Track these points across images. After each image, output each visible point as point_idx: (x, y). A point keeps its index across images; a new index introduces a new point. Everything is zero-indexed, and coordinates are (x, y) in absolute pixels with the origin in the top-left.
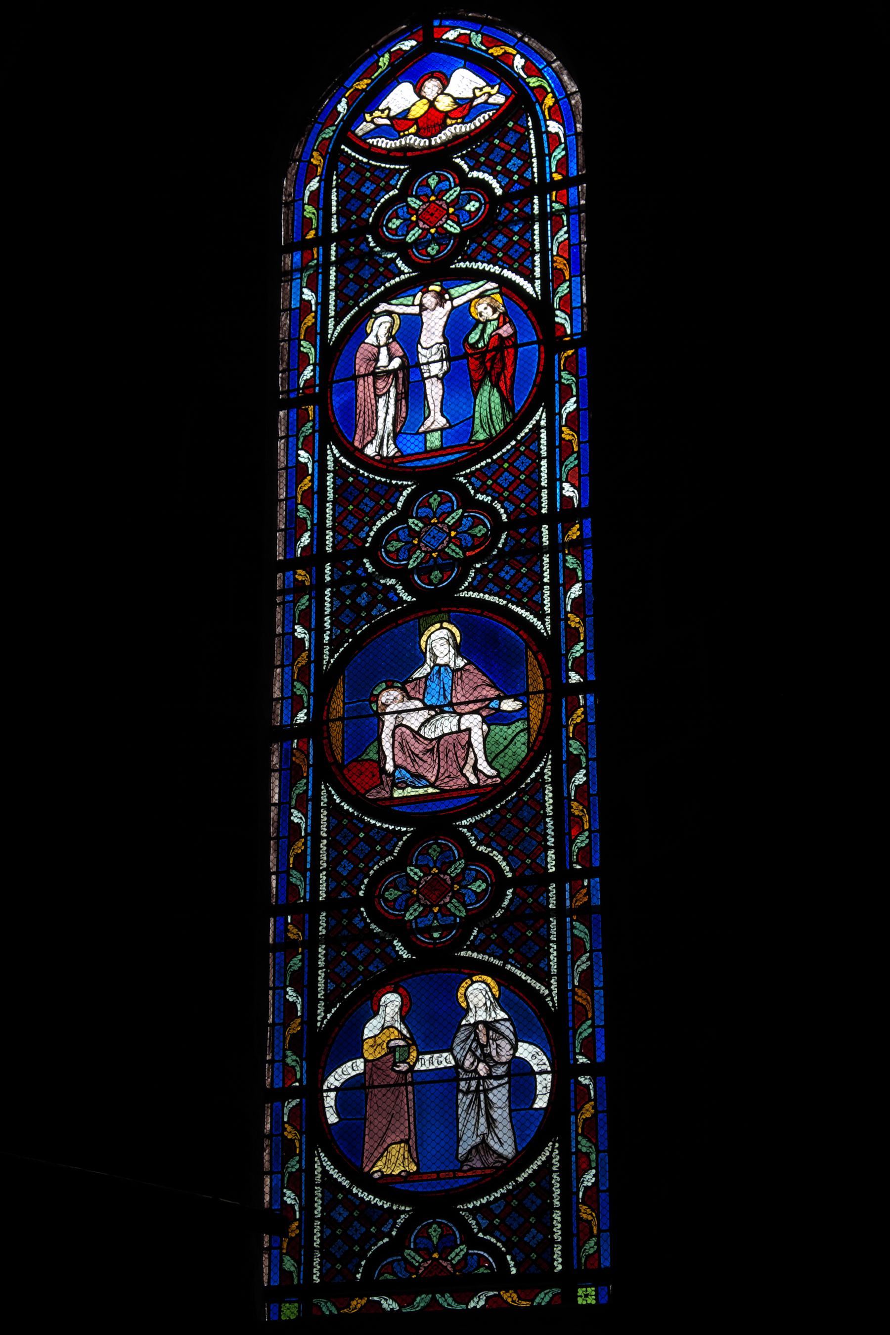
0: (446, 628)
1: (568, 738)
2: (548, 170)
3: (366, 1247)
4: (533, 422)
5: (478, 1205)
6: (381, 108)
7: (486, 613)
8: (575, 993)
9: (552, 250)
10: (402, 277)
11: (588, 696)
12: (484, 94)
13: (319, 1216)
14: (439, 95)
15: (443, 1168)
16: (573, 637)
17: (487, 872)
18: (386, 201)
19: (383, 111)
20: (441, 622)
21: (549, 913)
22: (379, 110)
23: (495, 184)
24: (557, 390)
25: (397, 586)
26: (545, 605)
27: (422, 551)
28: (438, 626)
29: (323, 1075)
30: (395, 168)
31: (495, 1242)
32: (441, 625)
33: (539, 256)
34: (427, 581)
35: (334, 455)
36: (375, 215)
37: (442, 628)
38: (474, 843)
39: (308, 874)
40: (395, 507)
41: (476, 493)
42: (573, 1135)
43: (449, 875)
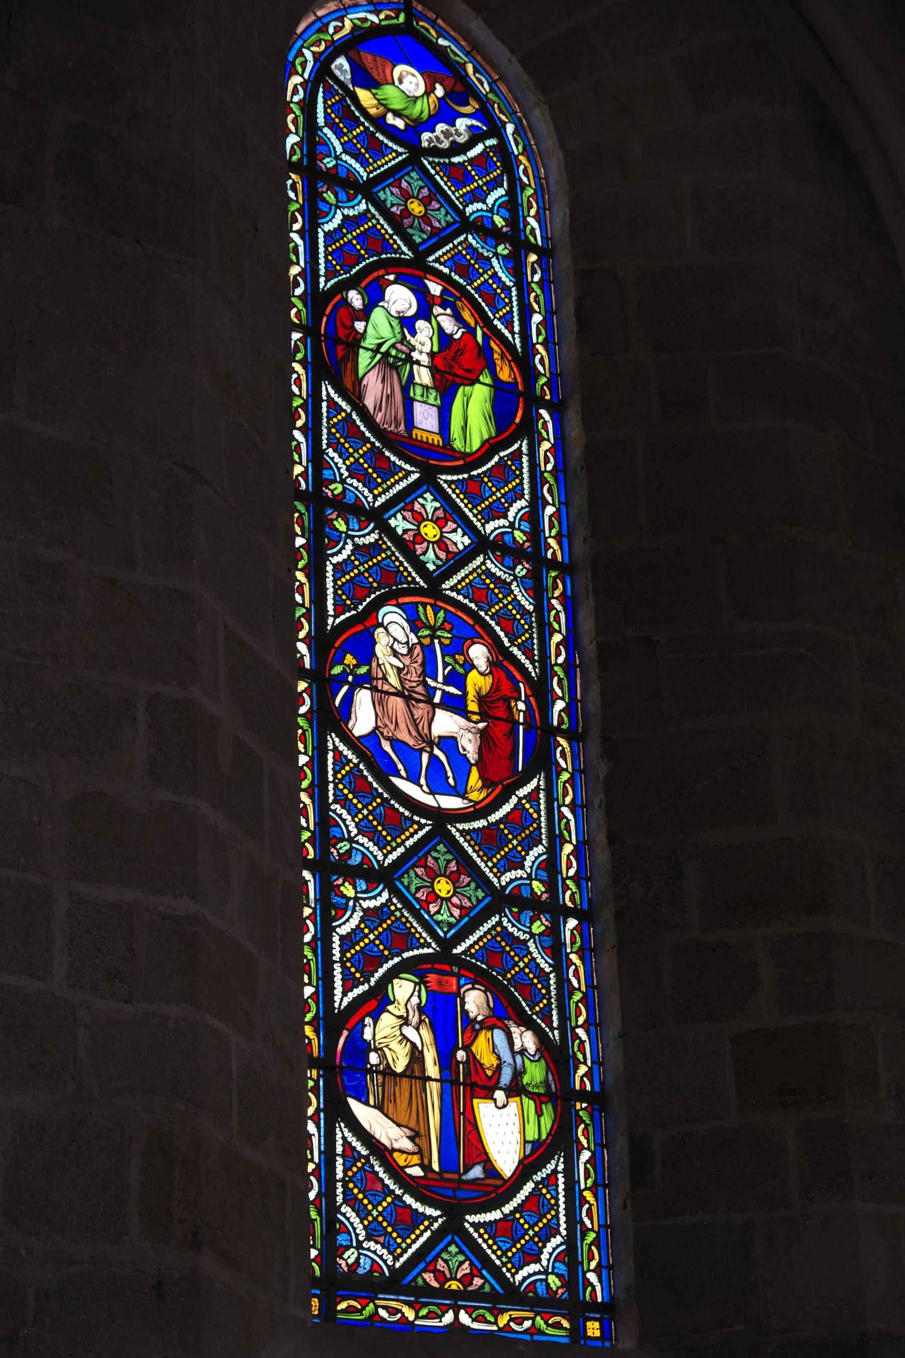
38: (552, 976)
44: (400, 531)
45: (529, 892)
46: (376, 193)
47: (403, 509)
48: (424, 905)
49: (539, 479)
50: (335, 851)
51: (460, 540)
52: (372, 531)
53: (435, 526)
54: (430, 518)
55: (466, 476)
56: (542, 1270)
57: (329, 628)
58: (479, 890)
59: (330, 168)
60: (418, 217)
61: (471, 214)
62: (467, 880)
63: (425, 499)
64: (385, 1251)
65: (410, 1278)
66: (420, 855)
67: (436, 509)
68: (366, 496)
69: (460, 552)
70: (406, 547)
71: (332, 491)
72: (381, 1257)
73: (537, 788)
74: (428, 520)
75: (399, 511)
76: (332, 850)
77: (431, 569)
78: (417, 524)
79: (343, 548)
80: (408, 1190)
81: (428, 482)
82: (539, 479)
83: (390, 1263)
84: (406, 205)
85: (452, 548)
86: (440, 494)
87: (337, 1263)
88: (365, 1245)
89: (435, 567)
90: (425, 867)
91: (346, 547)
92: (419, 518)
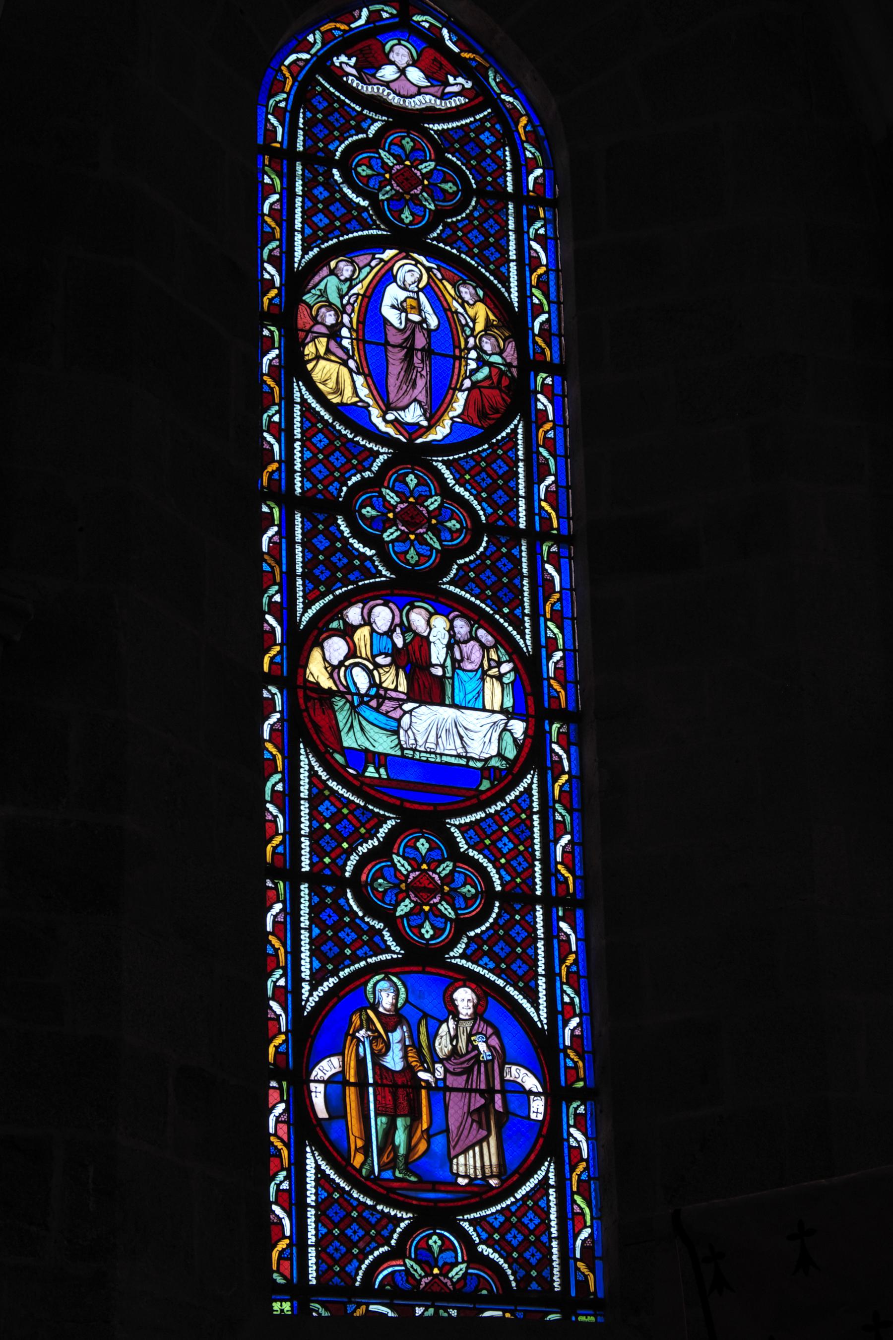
1: (569, 1126)
2: (536, 498)
3: (337, 435)
4: (512, 426)
8: (550, 686)
9: (560, 974)
10: (403, 1225)
12: (457, 84)
14: (408, 65)
16: (538, 310)
17: (470, 912)
21: (505, 197)
23: (495, 877)
24: (556, 946)
25: (384, 933)
26: (554, 1281)
29: (307, 1068)
33: (542, 942)
34: (396, 216)
39: (285, 224)
40: (380, 931)
41: (468, 937)
42: (565, 1127)
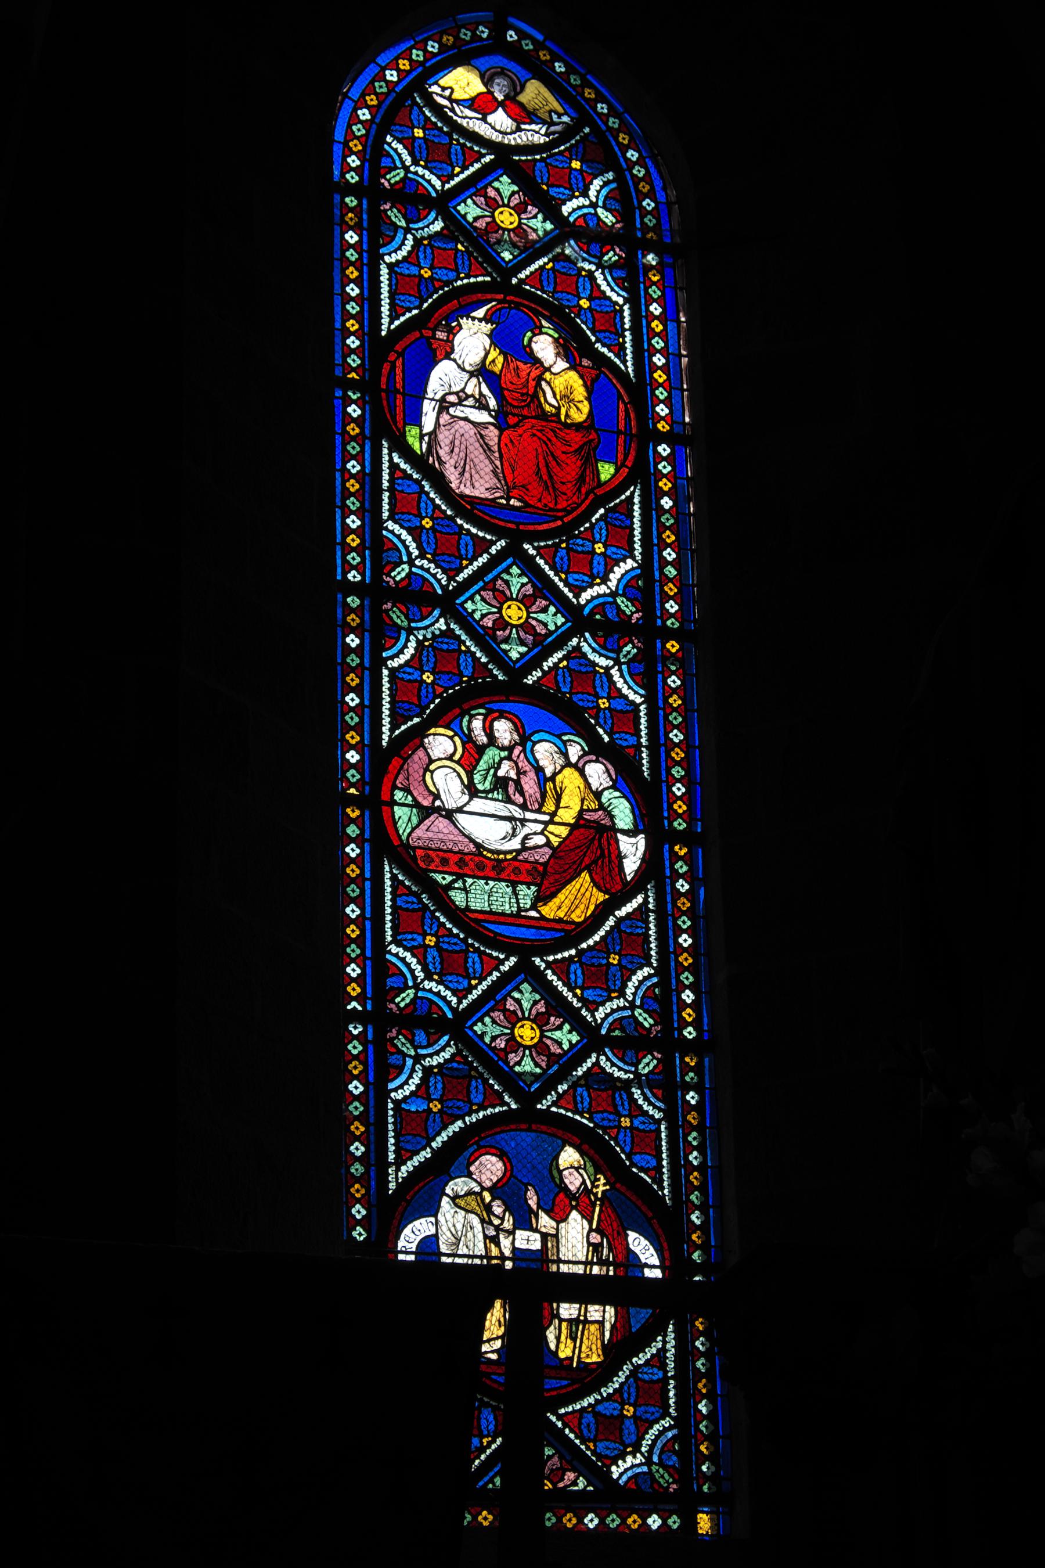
0: (454, 743)
5: (611, 1392)
6: (442, 82)
7: (513, 526)
11: (566, 214)
13: (490, 666)
15: (523, 1134)
18: (480, 529)
19: (444, 89)
20: (456, 734)
22: (439, 86)
27: (397, 1037)
28: (451, 733)
30: (484, 538)
31: (556, 957)
32: (453, 736)
35: (398, 1170)
36: (432, 303)
37: (451, 738)
38: (642, 707)
43: (669, 1484)
44: (470, 218)
45: (615, 612)
46: (462, 604)
47: (483, 589)
48: (491, 585)
49: (645, 330)
50: (392, 580)
51: (566, 1037)
52: (448, 1044)
53: (534, 1026)
54: (514, 596)
55: (573, 952)
56: (627, 1005)
57: (383, 333)
58: (559, 615)
59: (397, 183)
60: (504, 205)
61: (570, 214)
62: (535, 211)
63: (521, 992)
64: (441, 988)
65: (481, 1483)
66: (486, 579)
67: (523, 585)
68: (438, 578)
69: (566, 1052)
70: (485, 638)
71: (389, 181)
72: (434, 576)
73: (643, 907)
74: (512, 599)
75: (478, 592)
76: (383, 181)
77: (505, 177)
78: (510, 1026)
79: (405, 646)
80: (460, 511)
81: (517, 671)
82: (645, 330)
83: (444, 583)
84: (493, 216)
85: (555, 1049)
86: (529, 567)
87: (384, 581)
88: (418, 562)
89: (511, 257)
90: (505, 1011)
91: (409, 644)
92: (493, 205)
